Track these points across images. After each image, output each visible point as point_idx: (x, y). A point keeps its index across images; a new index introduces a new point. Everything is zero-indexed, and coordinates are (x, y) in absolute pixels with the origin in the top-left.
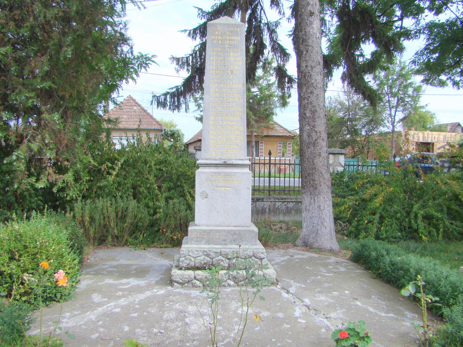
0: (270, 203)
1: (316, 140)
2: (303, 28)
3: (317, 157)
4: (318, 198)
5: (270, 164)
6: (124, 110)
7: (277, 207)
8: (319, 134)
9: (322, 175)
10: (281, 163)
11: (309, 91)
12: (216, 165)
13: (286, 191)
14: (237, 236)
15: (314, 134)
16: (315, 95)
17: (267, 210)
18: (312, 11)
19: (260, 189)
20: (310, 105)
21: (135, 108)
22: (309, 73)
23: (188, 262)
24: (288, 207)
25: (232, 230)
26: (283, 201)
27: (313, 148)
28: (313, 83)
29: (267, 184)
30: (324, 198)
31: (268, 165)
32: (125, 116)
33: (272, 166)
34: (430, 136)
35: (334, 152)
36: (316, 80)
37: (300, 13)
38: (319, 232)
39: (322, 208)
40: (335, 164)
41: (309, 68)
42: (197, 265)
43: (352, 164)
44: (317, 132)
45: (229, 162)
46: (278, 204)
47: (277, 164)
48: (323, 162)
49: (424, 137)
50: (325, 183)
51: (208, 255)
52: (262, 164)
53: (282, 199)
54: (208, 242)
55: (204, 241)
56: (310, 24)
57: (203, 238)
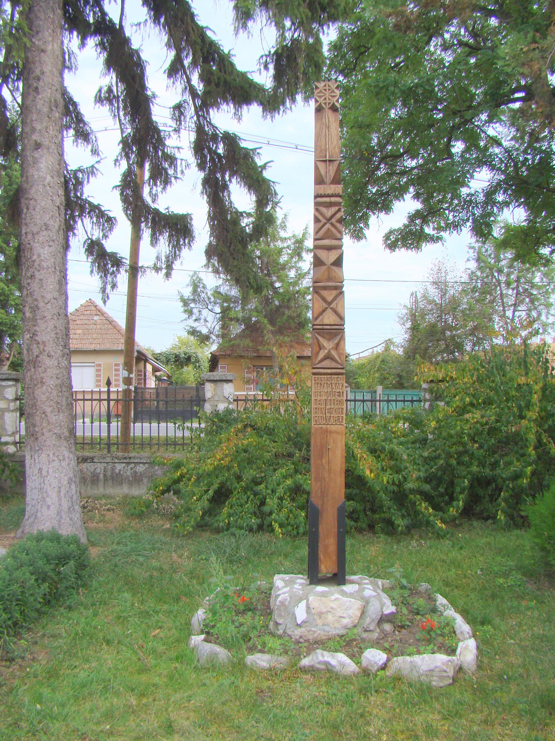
0: (106, 464)
1: (37, 356)
3: (39, 385)
4: (39, 457)
7: (117, 471)
8: (41, 347)
9: (46, 416)
11: (29, 275)
13: (136, 444)
15: (35, 346)
16: (37, 280)
17: (101, 476)
18: (39, 141)
19: (95, 441)
20: (30, 298)
21: (96, 318)
22: (29, 244)
24: (136, 472)
26: (128, 461)
27: (33, 370)
28: (35, 261)
29: (104, 434)
30: (49, 455)
31: (105, 403)
32: (80, 331)
35: (212, 378)
36: (39, 256)
38: (39, 514)
39: (44, 473)
40: (216, 398)
41: (30, 236)
43: (394, 399)
44: (38, 343)
48: (47, 394)
50: (50, 431)
53: (125, 458)
56: (34, 163)
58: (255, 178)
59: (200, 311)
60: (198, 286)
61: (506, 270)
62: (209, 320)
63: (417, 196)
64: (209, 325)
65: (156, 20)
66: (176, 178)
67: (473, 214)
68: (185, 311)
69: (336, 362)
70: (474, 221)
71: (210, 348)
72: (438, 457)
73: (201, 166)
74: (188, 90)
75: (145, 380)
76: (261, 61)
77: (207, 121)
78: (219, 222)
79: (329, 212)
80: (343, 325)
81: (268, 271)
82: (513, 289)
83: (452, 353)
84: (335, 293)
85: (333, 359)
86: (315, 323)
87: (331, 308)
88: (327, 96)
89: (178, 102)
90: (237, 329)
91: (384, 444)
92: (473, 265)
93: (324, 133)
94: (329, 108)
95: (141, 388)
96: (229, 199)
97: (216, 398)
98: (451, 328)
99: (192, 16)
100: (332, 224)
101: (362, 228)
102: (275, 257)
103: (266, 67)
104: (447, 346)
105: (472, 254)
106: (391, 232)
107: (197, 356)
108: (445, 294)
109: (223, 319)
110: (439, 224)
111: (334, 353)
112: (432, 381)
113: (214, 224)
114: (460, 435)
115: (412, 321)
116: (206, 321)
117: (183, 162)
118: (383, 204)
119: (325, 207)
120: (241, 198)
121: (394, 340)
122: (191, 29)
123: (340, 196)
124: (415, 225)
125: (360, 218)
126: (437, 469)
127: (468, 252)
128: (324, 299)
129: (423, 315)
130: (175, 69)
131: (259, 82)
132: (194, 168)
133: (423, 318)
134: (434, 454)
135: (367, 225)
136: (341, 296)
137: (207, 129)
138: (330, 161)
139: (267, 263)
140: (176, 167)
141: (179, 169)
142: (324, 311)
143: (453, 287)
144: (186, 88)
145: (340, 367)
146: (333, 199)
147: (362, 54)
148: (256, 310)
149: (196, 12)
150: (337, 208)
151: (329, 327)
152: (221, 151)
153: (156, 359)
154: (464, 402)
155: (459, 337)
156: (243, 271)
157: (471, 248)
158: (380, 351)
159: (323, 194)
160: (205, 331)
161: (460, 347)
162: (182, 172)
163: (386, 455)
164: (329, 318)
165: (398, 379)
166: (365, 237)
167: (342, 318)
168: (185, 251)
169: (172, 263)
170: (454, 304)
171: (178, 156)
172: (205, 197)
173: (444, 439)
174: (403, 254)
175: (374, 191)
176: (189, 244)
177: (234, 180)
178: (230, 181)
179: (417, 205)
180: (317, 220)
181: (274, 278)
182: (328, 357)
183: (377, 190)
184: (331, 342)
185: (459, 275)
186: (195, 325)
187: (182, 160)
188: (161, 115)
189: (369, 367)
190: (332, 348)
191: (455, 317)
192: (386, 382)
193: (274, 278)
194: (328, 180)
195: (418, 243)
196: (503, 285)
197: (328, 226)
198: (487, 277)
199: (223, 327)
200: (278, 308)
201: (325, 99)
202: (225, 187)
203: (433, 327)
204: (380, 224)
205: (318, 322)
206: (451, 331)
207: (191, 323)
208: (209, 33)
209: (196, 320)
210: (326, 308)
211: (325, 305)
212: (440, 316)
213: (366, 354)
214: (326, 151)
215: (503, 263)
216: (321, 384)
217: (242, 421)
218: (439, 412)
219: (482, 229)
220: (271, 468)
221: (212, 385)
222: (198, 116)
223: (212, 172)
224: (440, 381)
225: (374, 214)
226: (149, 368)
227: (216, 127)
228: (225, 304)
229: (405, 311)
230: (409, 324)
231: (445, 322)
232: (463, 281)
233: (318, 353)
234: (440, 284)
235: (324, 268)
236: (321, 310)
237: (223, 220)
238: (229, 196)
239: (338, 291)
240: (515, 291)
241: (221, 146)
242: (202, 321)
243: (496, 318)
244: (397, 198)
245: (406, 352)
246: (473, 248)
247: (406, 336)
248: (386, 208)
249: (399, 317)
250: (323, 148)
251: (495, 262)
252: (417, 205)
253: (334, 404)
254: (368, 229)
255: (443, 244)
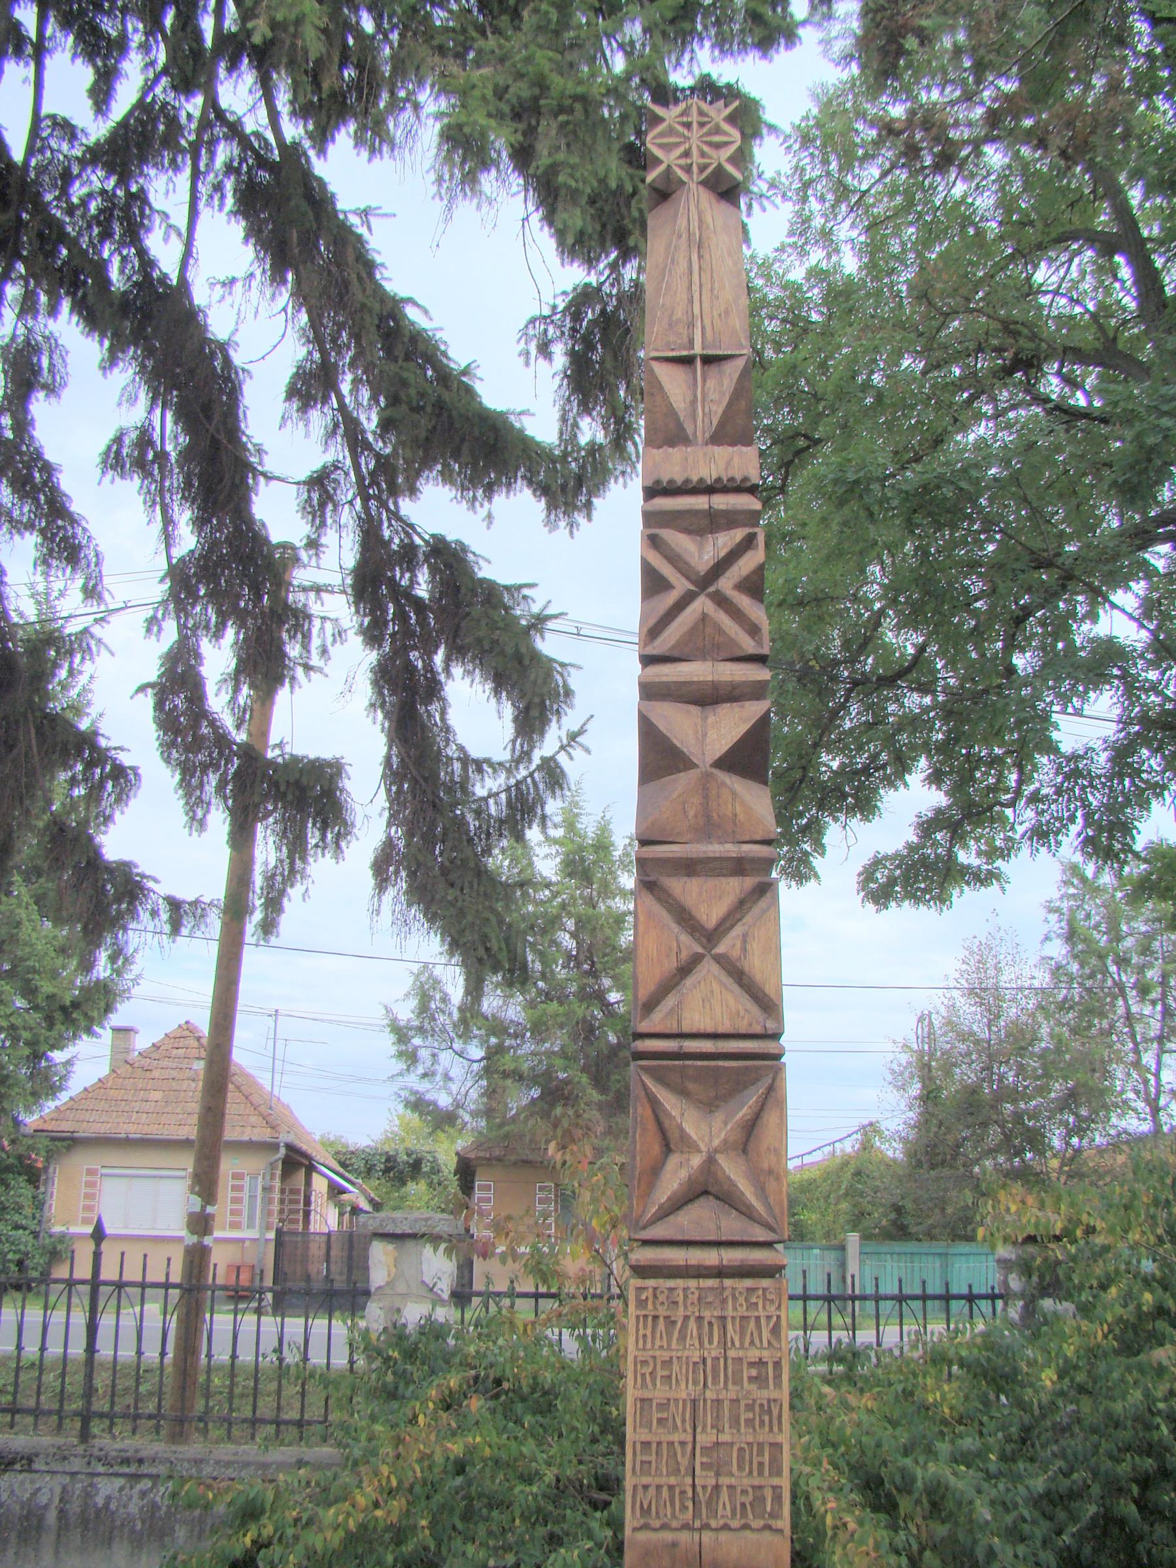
6: (156, 1074)
7: (100, 1501)
10: (882, 1291)
17: (52, 1517)
18: (296, 404)
32: (158, 1095)
35: (390, 1229)
40: (401, 1288)
46: (107, 1488)
52: (886, 1298)
53: (126, 1461)
58: (509, 650)
59: (434, 1055)
60: (431, 998)
61: (1135, 960)
62: (456, 1075)
63: (935, 778)
64: (454, 1088)
65: (277, 278)
66: (308, 668)
67: (1085, 805)
68: (401, 1054)
69: (747, 1213)
70: (1087, 817)
71: (453, 1142)
72: (1074, 1495)
73: (372, 636)
74: (341, 431)
75: (307, 1214)
76: (531, 332)
77: (388, 510)
78: (414, 782)
79: (703, 553)
80: (776, 1036)
81: (593, 964)
82: (1153, 1003)
83: (1019, 1152)
84: (734, 887)
85: (728, 1199)
86: (644, 1027)
87: (720, 960)
88: (695, 143)
89: (317, 465)
90: (519, 1099)
91: (908, 1461)
92: (1058, 950)
93: (683, 264)
94: (704, 183)
95: (294, 1233)
96: (443, 719)
97: (401, 1288)
98: (1014, 1095)
99: (369, 267)
100: (721, 601)
101: (806, 854)
102: (608, 932)
103: (544, 349)
104: (1008, 1138)
105: (1056, 925)
106: (877, 862)
107: (435, 1160)
108: (998, 1017)
109: (488, 1071)
110: (990, 841)
111: (732, 1170)
112: (1031, 1239)
113: (399, 791)
114: (1144, 1419)
115: (923, 1080)
116: (447, 1077)
117: (329, 626)
118: (857, 796)
119: (687, 531)
120: (474, 715)
121: (883, 1126)
122: (354, 276)
123: (752, 490)
124: (935, 844)
125: (804, 830)
126: (1079, 1536)
127: (1046, 921)
128: (685, 918)
129: (948, 1068)
130: (311, 387)
131: (538, 439)
132: (355, 641)
133: (947, 1072)
134: (1067, 1483)
135: (820, 848)
136: (763, 903)
137: (387, 534)
138: (708, 360)
139: (591, 946)
140: (307, 637)
141: (316, 642)
142: (685, 970)
143: (1013, 1000)
144: (336, 426)
145: (761, 1235)
146: (721, 502)
147: (799, 452)
148: (563, 1054)
149: (379, 259)
150: (739, 534)
151: (707, 1046)
152: (422, 591)
153: (343, 1165)
154: (1139, 1306)
155: (1034, 1116)
156: (470, 918)
157: (1051, 910)
158: (849, 1150)
159: (679, 479)
160: (444, 1101)
161: (1036, 1140)
162: (324, 651)
163: (918, 1502)
164: (708, 1005)
165: (893, 1216)
166: (816, 876)
167: (770, 1006)
168: (320, 866)
169: (282, 893)
170: (1020, 1040)
171: (315, 609)
172: (380, 715)
173: (1094, 1430)
174: (905, 916)
175: (835, 765)
176: (338, 846)
177: (457, 670)
178: (447, 670)
179: (937, 798)
180: (653, 583)
181: (607, 982)
182: (706, 1188)
183: (842, 764)
184: (719, 1116)
185: (1026, 972)
186: (423, 1086)
187: (324, 619)
188: (277, 513)
189: (825, 1186)
190: (726, 1147)
191: (1021, 1070)
192: (867, 1222)
193: (607, 982)
194: (702, 424)
195: (942, 886)
196: (1132, 994)
197: (702, 604)
198: (1092, 976)
199: (490, 1093)
200: (614, 1050)
201: (687, 154)
202: (433, 690)
203: (974, 1092)
204: (851, 845)
205: (656, 1021)
206: (1014, 1101)
207: (413, 1081)
208: (411, 313)
209: (425, 1075)
210: (696, 960)
211: (690, 945)
212: (989, 1068)
213: (817, 1157)
214: (691, 325)
215: (1129, 942)
216: (669, 1322)
217: (466, 1364)
218: (1063, 1337)
219: (1108, 838)
220: (541, 1531)
221: (390, 1247)
222: (366, 499)
223: (400, 651)
224: (1058, 1238)
225: (836, 819)
226: (320, 1185)
227: (412, 526)
228: (493, 1040)
229: (904, 1058)
230: (915, 1089)
231: (1000, 1080)
232: (1036, 984)
233: (655, 1170)
234: (985, 994)
235: (682, 782)
236: (671, 964)
237: (426, 779)
238: (443, 713)
239: (749, 882)
240: (1159, 1008)
241: (423, 576)
242: (438, 1078)
243: (1119, 1071)
244: (890, 783)
245: (911, 1154)
246: (1057, 910)
247: (911, 1114)
248: (865, 806)
249: (893, 1071)
250: (679, 313)
251: (1110, 941)
252: (937, 798)
253: (735, 1422)
254: (822, 854)
255: (1003, 890)
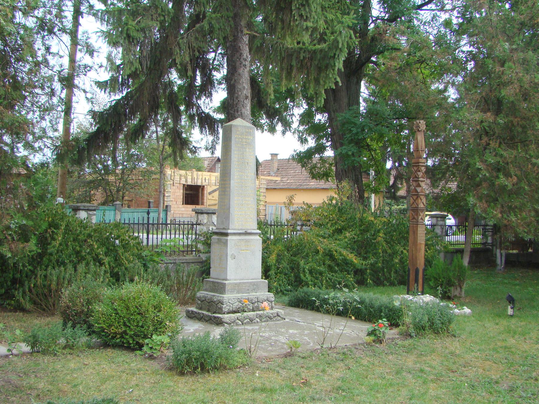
2: (240, 109)
5: (148, 224)
12: (240, 234)
14: (255, 287)
23: (228, 307)
25: (252, 282)
33: (150, 226)
34: (200, 177)
37: (236, 95)
40: (209, 223)
42: (234, 309)
45: (249, 231)
47: (155, 224)
49: (192, 179)
51: (240, 302)
54: (238, 292)
55: (236, 291)
57: (235, 289)
